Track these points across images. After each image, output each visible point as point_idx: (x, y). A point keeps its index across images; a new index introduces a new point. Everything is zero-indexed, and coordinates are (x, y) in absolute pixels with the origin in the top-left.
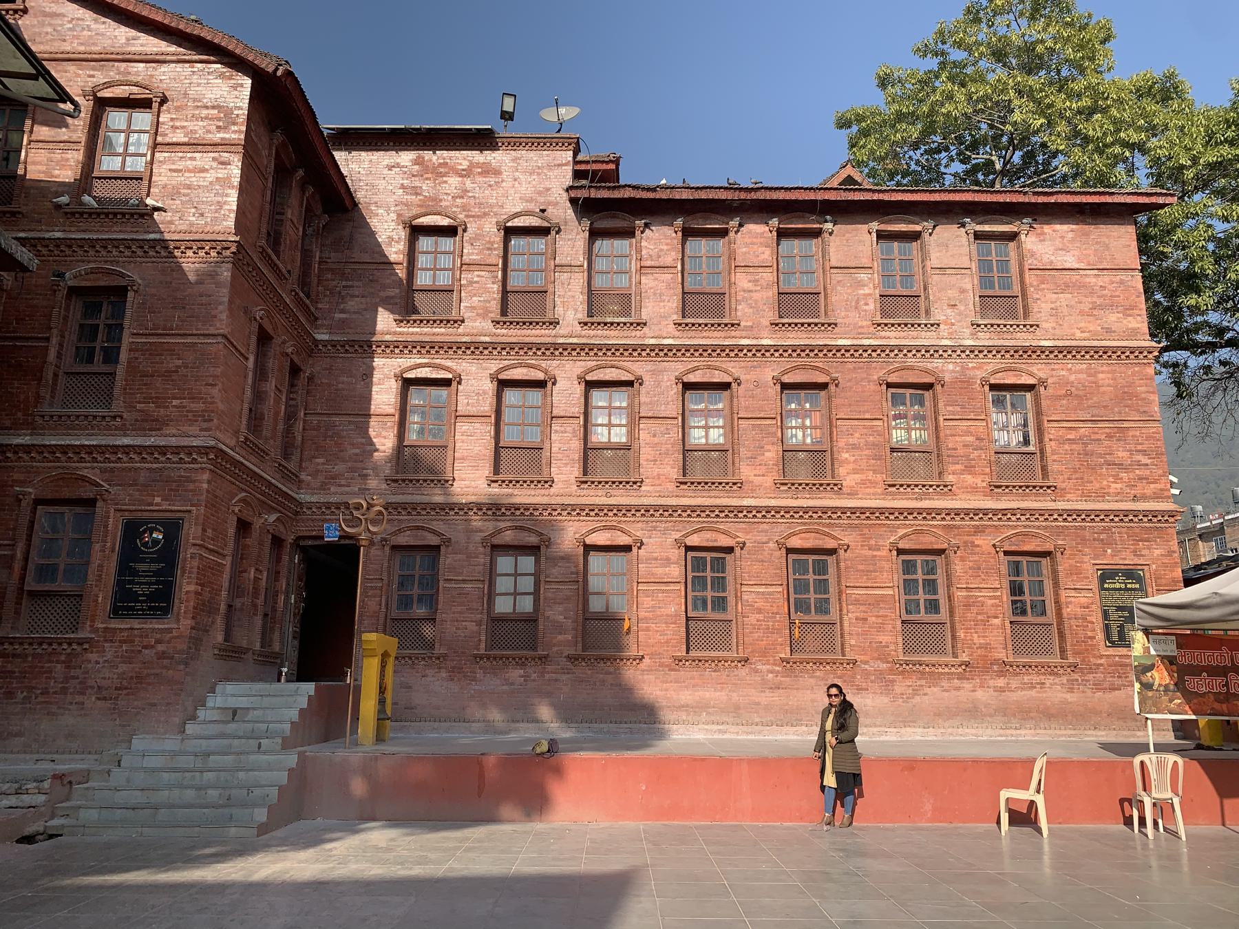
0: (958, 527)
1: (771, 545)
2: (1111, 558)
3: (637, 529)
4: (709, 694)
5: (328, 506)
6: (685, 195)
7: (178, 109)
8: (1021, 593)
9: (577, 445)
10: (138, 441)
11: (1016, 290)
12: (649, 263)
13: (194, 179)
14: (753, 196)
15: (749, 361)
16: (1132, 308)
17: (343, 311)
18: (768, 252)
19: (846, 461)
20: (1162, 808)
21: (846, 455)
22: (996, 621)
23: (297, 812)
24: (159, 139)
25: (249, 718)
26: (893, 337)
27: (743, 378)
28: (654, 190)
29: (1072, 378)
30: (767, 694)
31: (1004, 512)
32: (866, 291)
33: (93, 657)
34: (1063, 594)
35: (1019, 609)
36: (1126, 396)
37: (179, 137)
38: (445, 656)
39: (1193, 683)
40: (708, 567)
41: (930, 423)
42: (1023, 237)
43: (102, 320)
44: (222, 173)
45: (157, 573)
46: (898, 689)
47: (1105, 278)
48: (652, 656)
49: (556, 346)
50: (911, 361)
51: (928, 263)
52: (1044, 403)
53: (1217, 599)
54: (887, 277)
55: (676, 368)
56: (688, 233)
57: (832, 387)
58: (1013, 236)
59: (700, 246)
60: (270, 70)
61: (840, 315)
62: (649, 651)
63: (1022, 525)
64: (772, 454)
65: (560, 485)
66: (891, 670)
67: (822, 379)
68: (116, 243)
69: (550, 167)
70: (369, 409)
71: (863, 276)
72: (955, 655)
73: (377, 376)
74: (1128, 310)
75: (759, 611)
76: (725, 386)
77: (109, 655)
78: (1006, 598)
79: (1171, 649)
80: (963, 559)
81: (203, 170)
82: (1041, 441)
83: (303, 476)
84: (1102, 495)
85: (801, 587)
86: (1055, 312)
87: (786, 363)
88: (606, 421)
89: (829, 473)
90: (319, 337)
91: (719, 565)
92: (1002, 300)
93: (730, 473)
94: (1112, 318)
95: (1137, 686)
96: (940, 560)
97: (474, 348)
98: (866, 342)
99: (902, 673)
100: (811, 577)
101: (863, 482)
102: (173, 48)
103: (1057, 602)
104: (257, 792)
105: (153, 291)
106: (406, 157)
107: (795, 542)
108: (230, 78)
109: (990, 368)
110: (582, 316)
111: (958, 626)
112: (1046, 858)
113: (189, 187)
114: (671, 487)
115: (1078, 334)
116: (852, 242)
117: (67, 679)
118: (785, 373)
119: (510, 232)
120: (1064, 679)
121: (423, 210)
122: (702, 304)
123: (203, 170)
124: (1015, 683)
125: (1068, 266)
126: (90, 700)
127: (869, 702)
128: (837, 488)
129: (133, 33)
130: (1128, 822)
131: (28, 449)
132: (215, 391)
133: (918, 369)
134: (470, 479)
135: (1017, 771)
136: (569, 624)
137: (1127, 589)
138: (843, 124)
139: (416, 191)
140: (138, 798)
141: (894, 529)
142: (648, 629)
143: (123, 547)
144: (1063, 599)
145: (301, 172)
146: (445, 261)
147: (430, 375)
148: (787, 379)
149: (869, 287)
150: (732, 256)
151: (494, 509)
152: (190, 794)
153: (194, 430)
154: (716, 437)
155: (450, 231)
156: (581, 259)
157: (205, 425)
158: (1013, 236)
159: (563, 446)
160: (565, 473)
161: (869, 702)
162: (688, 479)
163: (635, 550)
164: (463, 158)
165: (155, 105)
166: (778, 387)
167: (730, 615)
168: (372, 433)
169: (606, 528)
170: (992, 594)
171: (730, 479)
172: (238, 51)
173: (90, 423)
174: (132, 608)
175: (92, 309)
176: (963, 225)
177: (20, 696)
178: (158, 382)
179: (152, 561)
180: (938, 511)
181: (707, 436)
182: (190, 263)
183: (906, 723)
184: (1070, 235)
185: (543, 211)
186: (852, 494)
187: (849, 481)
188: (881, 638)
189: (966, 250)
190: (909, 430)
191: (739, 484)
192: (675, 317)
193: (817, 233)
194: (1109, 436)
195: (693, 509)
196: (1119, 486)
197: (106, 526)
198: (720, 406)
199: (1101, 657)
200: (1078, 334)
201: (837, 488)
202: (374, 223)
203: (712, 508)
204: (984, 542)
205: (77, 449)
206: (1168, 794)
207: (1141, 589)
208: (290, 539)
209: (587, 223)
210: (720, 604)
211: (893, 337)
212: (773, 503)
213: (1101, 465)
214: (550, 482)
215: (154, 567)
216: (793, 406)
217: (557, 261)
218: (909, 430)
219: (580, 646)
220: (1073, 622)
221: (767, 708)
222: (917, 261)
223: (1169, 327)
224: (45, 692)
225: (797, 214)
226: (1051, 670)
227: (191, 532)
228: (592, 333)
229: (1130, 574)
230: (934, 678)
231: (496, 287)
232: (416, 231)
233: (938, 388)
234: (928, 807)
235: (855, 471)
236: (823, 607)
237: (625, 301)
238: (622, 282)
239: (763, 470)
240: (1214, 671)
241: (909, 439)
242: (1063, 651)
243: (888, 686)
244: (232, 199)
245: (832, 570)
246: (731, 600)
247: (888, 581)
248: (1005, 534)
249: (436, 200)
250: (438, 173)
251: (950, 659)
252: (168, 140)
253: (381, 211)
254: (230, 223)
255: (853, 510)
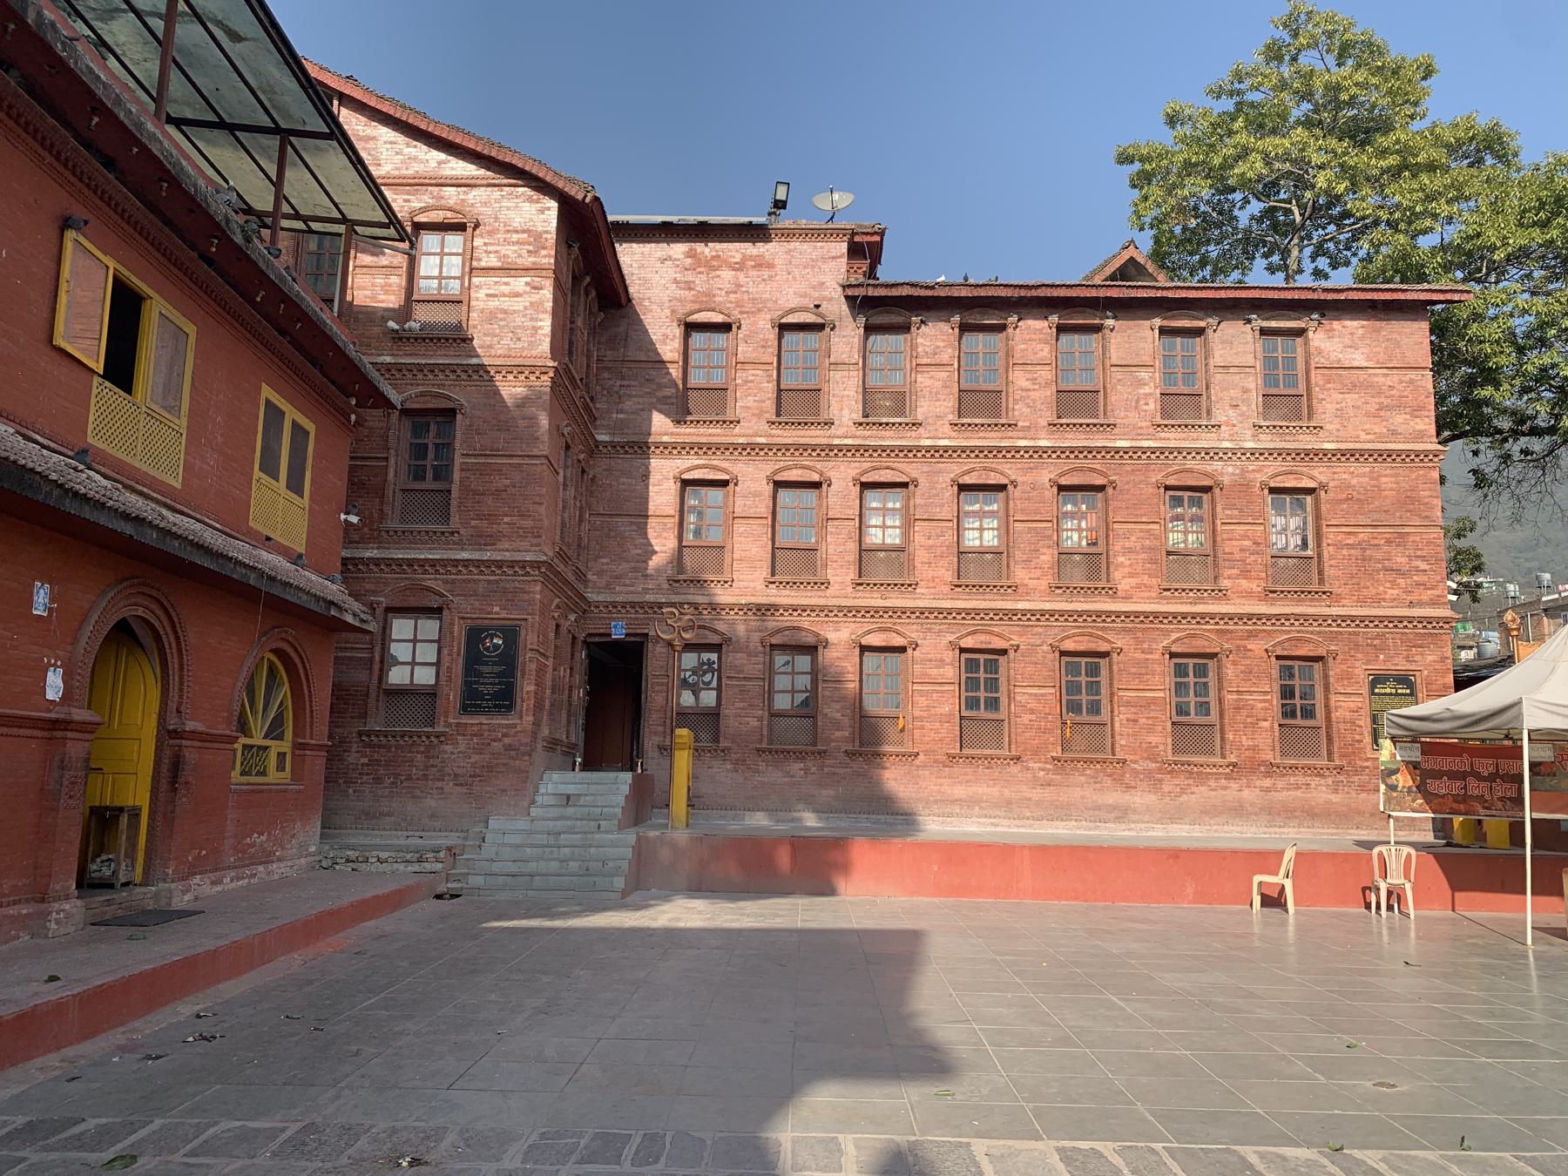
0: (1231, 632)
1: (1045, 648)
2: (1381, 664)
3: (911, 631)
4: (981, 790)
5: (614, 605)
6: (964, 292)
7: (491, 233)
8: (1292, 696)
9: (852, 546)
10: (476, 556)
11: (1302, 389)
12: (924, 361)
13: (506, 303)
14: (1034, 293)
15: (1026, 462)
16: (1420, 408)
17: (622, 412)
18: (1047, 349)
19: (1122, 565)
20: (1395, 895)
21: (1121, 559)
22: (1266, 724)
23: (644, 880)
24: (475, 264)
25: (581, 802)
26: (1173, 439)
27: (1020, 479)
28: (933, 288)
29: (1354, 481)
30: (1039, 790)
31: (1278, 617)
32: (1147, 390)
33: (449, 748)
34: (1333, 698)
35: (1289, 713)
36: (1408, 501)
37: (493, 261)
38: (729, 749)
39: (1434, 786)
40: (982, 669)
41: (1207, 526)
42: (1311, 334)
43: (431, 439)
44: (535, 297)
45: (499, 675)
46: (1166, 788)
47: (1394, 378)
48: (926, 753)
49: (831, 447)
50: (1190, 464)
51: (1211, 362)
52: (1323, 508)
53: (1448, 715)
54: (1168, 376)
55: (954, 469)
56: (964, 328)
57: (1110, 490)
58: (1301, 332)
59: (978, 341)
60: (580, 197)
61: (1119, 415)
62: (923, 747)
63: (1295, 630)
64: (1047, 557)
65: (837, 587)
66: (1160, 769)
67: (1099, 481)
68: (443, 368)
69: (824, 259)
70: (647, 509)
71: (1144, 374)
72: (1223, 757)
73: (654, 478)
74: (1416, 411)
75: (1032, 711)
76: (1002, 488)
77: (462, 748)
78: (1276, 701)
79: (1415, 754)
80: (1235, 663)
81: (517, 295)
82: (1319, 546)
83: (589, 576)
84: (1378, 600)
85: (1073, 688)
86: (1340, 413)
87: (1064, 464)
88: (879, 523)
89: (1104, 576)
90: (600, 438)
91: (992, 667)
92: (1286, 400)
93: (1004, 575)
94: (1398, 419)
95: (1382, 787)
96: (1211, 664)
97: (750, 449)
98: (1146, 444)
99: (1170, 772)
100: (1083, 679)
101: (1138, 586)
102: (482, 172)
103: (1327, 706)
104: (611, 864)
105: (478, 413)
106: (679, 249)
107: (1069, 645)
108: (538, 201)
109: (1270, 471)
110: (858, 417)
111: (1227, 728)
112: (1291, 928)
113: (505, 312)
114: (946, 589)
115: (1363, 436)
116: (1134, 340)
117: (426, 768)
118: (1061, 475)
119: (784, 328)
120: (1330, 781)
121: (697, 306)
122: (980, 403)
123: (517, 295)
124: (1280, 784)
125: (1356, 364)
126: (449, 786)
127: (1137, 799)
128: (1112, 592)
129: (442, 156)
130: (1368, 906)
131: (377, 562)
132: (542, 510)
133: (1198, 470)
134: (744, 581)
135: (1268, 860)
136: (846, 721)
137: (1397, 694)
138: (1125, 159)
139: (689, 286)
140: (513, 868)
141: (1167, 633)
142: (922, 728)
143: (467, 651)
144: (1332, 703)
145: (588, 279)
146: (717, 358)
147: (711, 477)
148: (1063, 481)
149: (1150, 386)
150: (1009, 354)
151: (763, 610)
152: (554, 866)
153: (525, 544)
154: (990, 539)
155: (725, 327)
156: (856, 357)
157: (535, 541)
158: (1301, 332)
159: (838, 548)
160: (840, 575)
161: (1137, 799)
162: (963, 581)
163: (910, 651)
164: (735, 250)
165: (469, 230)
166: (1055, 489)
167: (1002, 715)
168: (651, 533)
169: (881, 630)
170: (1264, 698)
171: (1005, 582)
172: (548, 179)
173: (432, 538)
174: (480, 706)
175: (418, 430)
176: (1249, 321)
177: (388, 781)
178: (489, 500)
179: (495, 664)
180: (1212, 616)
181: (981, 537)
182: (511, 389)
183: (1172, 820)
184: (1360, 331)
185: (817, 306)
186: (1127, 598)
187: (1124, 585)
188: (1150, 739)
189: (1250, 347)
190: (1186, 533)
191: (1014, 588)
192: (951, 417)
193: (1097, 329)
194: (1389, 542)
195: (968, 612)
196: (1395, 592)
197: (452, 633)
198: (995, 507)
199: (1367, 759)
200: (1363, 436)
201: (1112, 592)
202: (647, 319)
203: (986, 611)
204: (1257, 646)
205: (422, 563)
206: (1402, 881)
207: (1412, 694)
208: (582, 636)
209: (862, 320)
210: (993, 704)
211: (1173, 439)
212: (1047, 606)
213: (1378, 571)
214: (826, 584)
215: (497, 669)
216: (1069, 507)
217: (832, 360)
218: (1186, 533)
219: (857, 743)
220: (1342, 726)
221: (1038, 804)
222: (1200, 357)
223: (1459, 419)
224: (409, 778)
225: (1076, 310)
226: (1318, 772)
227: (529, 638)
228: (867, 433)
229: (1404, 680)
230: (1201, 778)
231: (770, 387)
232: (690, 328)
233: (1217, 491)
234: (1190, 890)
235: (1131, 575)
236: (1095, 708)
237: (901, 401)
238: (897, 380)
239: (1038, 573)
240: (1453, 775)
241: (1185, 541)
242: (1330, 753)
243: (1156, 785)
244: (546, 324)
245: (1104, 672)
246: (1004, 701)
247: (1160, 685)
248: (1279, 639)
249: (709, 294)
250: (711, 265)
251: (1218, 760)
252: (483, 264)
253: (654, 307)
254: (545, 346)
255: (1127, 615)
